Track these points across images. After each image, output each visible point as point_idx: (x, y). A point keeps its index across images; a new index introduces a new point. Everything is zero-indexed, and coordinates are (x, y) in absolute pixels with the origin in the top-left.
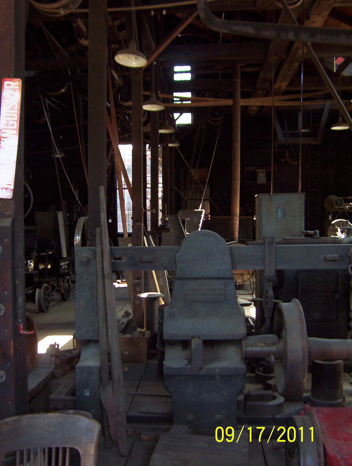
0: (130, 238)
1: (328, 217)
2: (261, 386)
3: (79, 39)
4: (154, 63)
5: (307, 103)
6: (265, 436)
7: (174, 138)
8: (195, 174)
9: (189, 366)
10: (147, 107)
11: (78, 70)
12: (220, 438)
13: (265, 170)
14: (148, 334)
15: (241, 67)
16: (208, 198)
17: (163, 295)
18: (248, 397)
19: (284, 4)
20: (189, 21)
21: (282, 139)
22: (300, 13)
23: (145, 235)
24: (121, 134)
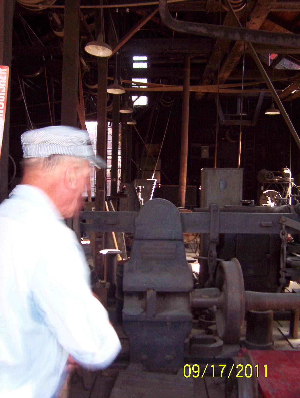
0: (94, 202)
2: (203, 331)
3: (53, 30)
4: (117, 53)
5: (246, 91)
6: (226, 371)
7: (131, 117)
8: (149, 148)
9: (144, 314)
10: (110, 91)
11: (51, 56)
12: (187, 374)
13: (208, 147)
14: (108, 284)
15: (191, 59)
16: (159, 169)
17: (121, 252)
18: (193, 340)
19: (229, 7)
20: (149, 18)
21: (223, 121)
22: (243, 15)
23: (106, 200)
24: (87, 112)
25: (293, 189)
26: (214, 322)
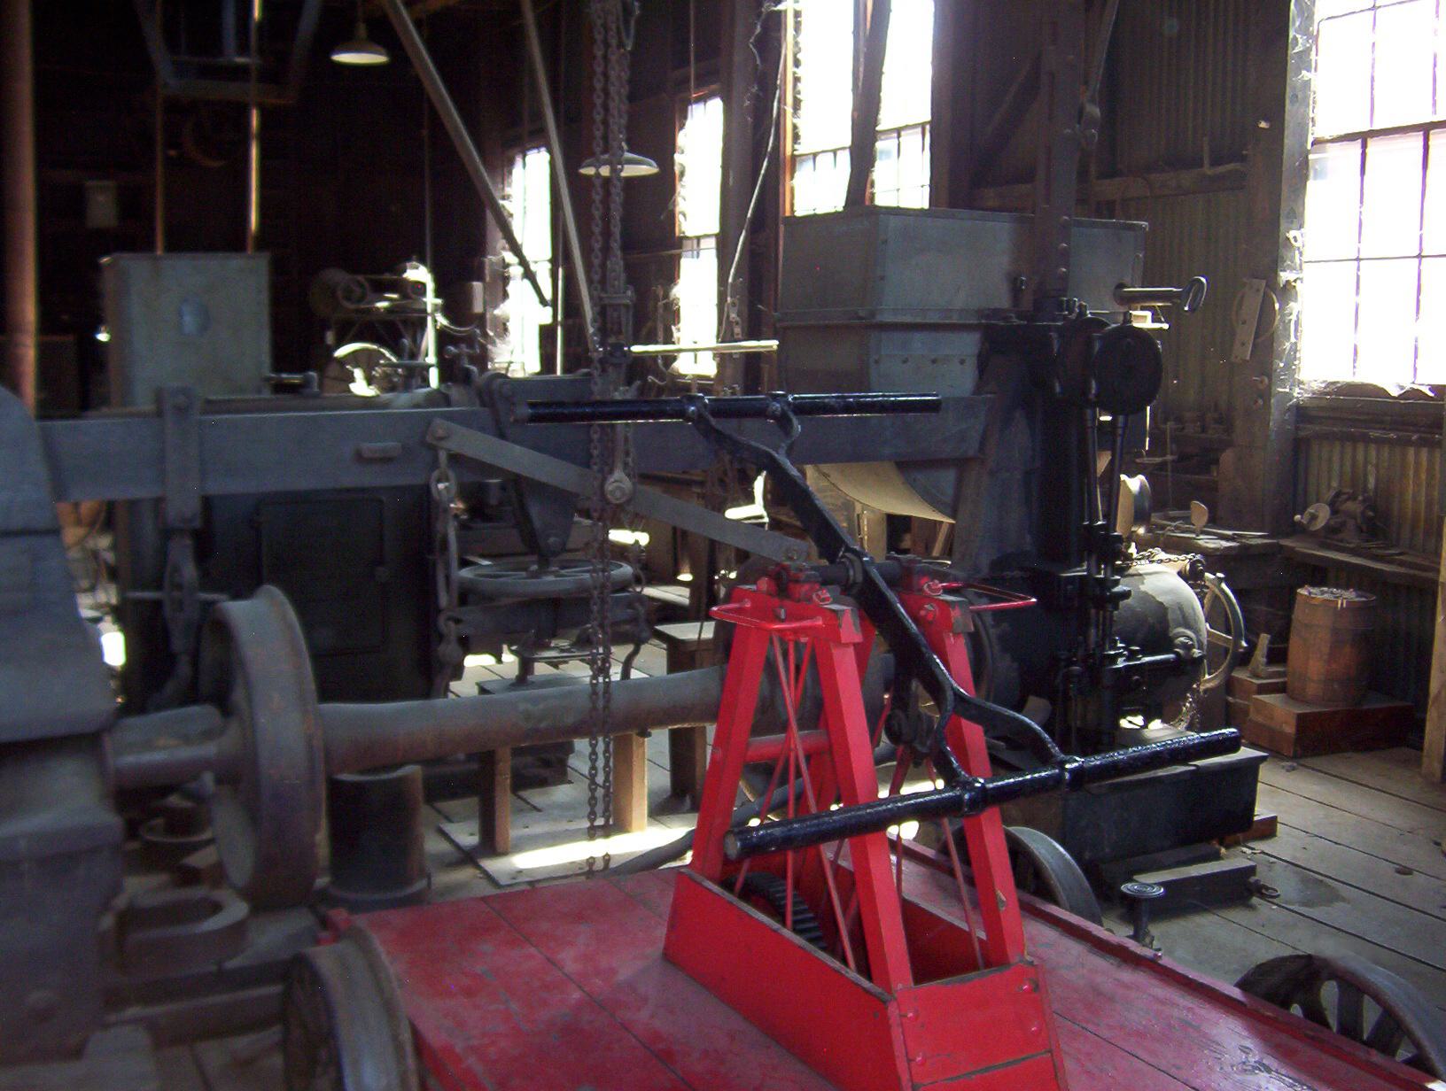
1: (322, 339)
18: (131, 918)
25: (443, 337)
26: (207, 835)
